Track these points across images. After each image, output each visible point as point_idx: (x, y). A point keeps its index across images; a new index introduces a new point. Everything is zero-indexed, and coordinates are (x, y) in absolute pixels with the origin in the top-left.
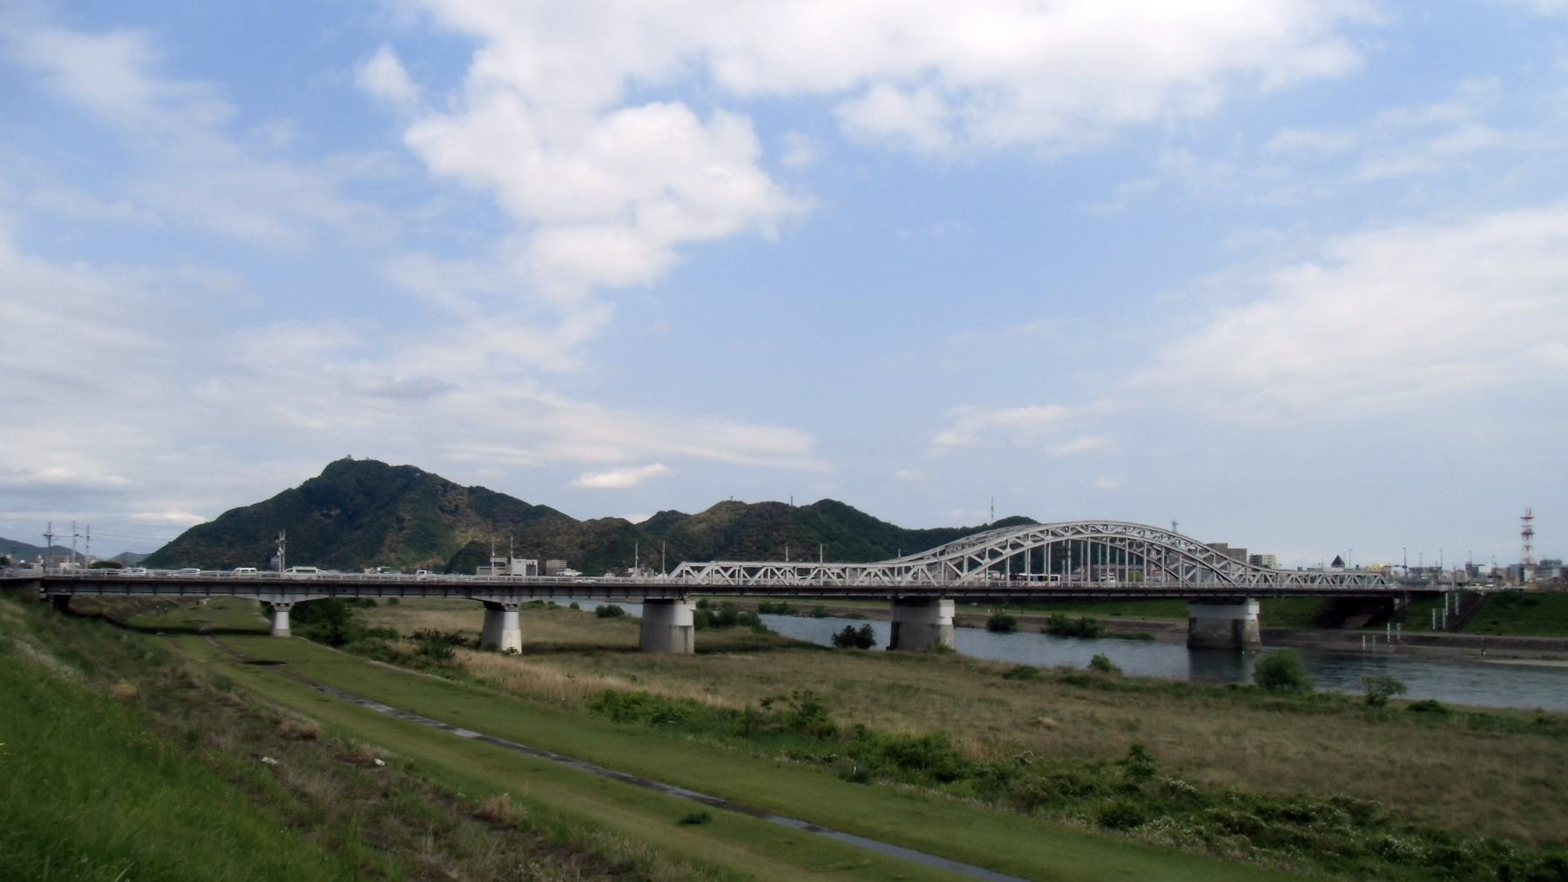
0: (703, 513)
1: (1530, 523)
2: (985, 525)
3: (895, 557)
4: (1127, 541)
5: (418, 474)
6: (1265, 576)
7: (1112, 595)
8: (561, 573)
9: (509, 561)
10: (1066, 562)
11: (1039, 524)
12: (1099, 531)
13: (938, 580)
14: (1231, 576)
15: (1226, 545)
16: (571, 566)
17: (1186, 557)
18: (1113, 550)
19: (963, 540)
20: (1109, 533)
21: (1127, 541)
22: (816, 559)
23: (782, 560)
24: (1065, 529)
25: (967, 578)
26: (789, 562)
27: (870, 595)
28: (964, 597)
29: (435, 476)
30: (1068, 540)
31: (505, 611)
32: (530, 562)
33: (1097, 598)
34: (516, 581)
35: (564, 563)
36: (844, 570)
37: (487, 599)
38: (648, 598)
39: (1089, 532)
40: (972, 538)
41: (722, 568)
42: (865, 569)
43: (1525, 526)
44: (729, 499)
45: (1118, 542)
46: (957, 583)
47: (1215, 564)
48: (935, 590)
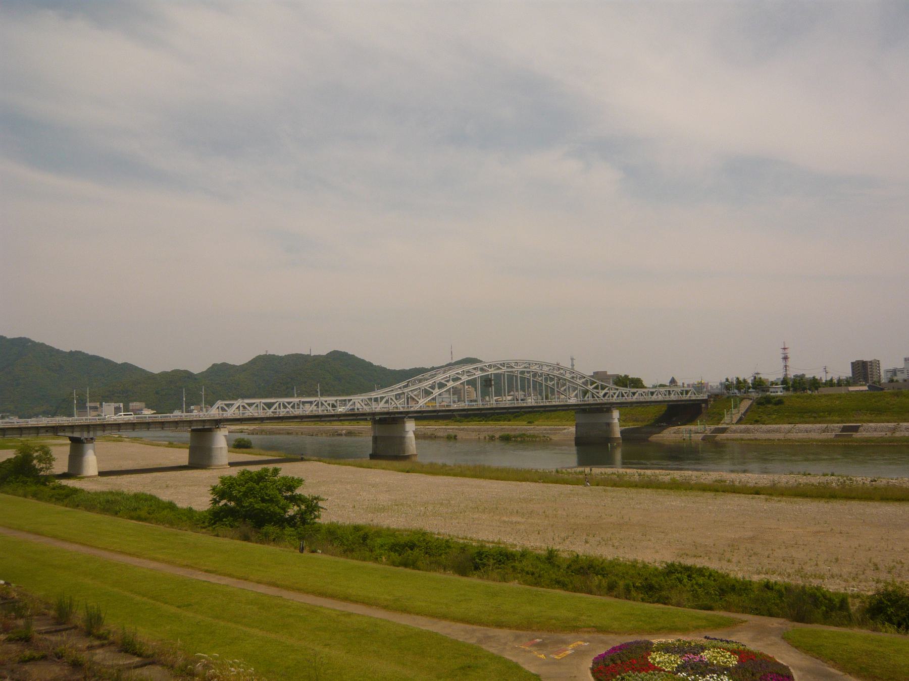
0: (246, 364)
1: (787, 351)
2: (433, 367)
3: (373, 390)
4: (531, 373)
5: (30, 344)
6: (622, 393)
7: (510, 411)
8: (140, 412)
9: (101, 405)
10: (492, 389)
11: (480, 361)
12: (512, 367)
13: (399, 406)
14: (600, 394)
15: (606, 372)
16: (148, 407)
17: (570, 382)
18: (523, 379)
19: (420, 377)
20: (520, 368)
21: (531, 373)
22: (315, 395)
23: (292, 396)
24: (503, 365)
25: (422, 403)
26: (297, 397)
27: (355, 418)
28: (421, 416)
29: (43, 344)
30: (492, 374)
31: (84, 443)
32: (117, 405)
33: (539, 411)
34: (60, 422)
35: (142, 405)
36: (336, 401)
37: (70, 435)
38: (192, 428)
39: (506, 368)
40: (427, 375)
41: (246, 403)
42: (351, 400)
43: (784, 354)
44: (265, 353)
45: (526, 374)
46: (416, 408)
47: (589, 386)
48: (401, 413)
